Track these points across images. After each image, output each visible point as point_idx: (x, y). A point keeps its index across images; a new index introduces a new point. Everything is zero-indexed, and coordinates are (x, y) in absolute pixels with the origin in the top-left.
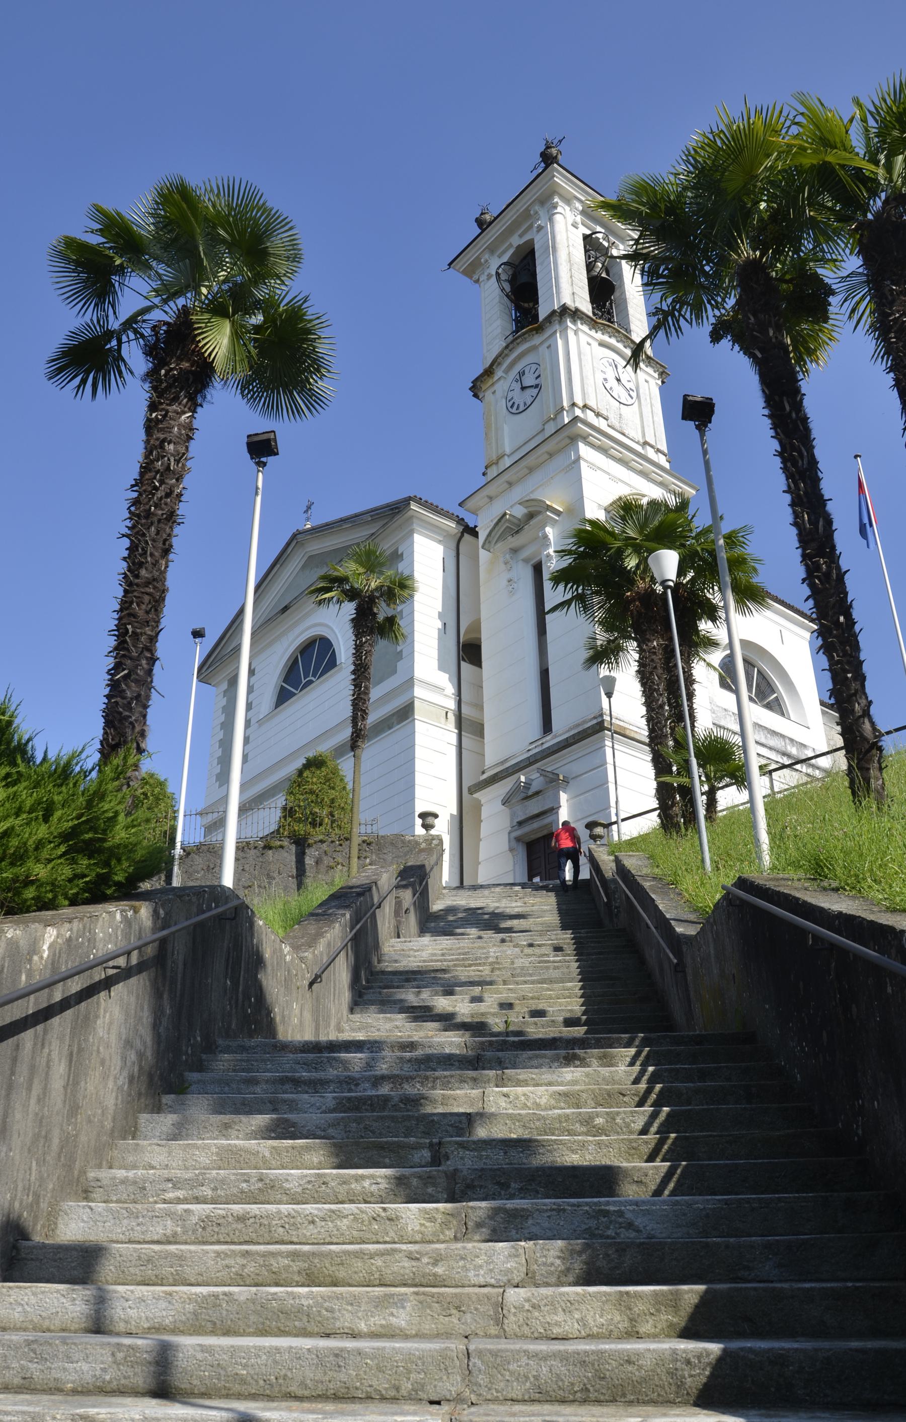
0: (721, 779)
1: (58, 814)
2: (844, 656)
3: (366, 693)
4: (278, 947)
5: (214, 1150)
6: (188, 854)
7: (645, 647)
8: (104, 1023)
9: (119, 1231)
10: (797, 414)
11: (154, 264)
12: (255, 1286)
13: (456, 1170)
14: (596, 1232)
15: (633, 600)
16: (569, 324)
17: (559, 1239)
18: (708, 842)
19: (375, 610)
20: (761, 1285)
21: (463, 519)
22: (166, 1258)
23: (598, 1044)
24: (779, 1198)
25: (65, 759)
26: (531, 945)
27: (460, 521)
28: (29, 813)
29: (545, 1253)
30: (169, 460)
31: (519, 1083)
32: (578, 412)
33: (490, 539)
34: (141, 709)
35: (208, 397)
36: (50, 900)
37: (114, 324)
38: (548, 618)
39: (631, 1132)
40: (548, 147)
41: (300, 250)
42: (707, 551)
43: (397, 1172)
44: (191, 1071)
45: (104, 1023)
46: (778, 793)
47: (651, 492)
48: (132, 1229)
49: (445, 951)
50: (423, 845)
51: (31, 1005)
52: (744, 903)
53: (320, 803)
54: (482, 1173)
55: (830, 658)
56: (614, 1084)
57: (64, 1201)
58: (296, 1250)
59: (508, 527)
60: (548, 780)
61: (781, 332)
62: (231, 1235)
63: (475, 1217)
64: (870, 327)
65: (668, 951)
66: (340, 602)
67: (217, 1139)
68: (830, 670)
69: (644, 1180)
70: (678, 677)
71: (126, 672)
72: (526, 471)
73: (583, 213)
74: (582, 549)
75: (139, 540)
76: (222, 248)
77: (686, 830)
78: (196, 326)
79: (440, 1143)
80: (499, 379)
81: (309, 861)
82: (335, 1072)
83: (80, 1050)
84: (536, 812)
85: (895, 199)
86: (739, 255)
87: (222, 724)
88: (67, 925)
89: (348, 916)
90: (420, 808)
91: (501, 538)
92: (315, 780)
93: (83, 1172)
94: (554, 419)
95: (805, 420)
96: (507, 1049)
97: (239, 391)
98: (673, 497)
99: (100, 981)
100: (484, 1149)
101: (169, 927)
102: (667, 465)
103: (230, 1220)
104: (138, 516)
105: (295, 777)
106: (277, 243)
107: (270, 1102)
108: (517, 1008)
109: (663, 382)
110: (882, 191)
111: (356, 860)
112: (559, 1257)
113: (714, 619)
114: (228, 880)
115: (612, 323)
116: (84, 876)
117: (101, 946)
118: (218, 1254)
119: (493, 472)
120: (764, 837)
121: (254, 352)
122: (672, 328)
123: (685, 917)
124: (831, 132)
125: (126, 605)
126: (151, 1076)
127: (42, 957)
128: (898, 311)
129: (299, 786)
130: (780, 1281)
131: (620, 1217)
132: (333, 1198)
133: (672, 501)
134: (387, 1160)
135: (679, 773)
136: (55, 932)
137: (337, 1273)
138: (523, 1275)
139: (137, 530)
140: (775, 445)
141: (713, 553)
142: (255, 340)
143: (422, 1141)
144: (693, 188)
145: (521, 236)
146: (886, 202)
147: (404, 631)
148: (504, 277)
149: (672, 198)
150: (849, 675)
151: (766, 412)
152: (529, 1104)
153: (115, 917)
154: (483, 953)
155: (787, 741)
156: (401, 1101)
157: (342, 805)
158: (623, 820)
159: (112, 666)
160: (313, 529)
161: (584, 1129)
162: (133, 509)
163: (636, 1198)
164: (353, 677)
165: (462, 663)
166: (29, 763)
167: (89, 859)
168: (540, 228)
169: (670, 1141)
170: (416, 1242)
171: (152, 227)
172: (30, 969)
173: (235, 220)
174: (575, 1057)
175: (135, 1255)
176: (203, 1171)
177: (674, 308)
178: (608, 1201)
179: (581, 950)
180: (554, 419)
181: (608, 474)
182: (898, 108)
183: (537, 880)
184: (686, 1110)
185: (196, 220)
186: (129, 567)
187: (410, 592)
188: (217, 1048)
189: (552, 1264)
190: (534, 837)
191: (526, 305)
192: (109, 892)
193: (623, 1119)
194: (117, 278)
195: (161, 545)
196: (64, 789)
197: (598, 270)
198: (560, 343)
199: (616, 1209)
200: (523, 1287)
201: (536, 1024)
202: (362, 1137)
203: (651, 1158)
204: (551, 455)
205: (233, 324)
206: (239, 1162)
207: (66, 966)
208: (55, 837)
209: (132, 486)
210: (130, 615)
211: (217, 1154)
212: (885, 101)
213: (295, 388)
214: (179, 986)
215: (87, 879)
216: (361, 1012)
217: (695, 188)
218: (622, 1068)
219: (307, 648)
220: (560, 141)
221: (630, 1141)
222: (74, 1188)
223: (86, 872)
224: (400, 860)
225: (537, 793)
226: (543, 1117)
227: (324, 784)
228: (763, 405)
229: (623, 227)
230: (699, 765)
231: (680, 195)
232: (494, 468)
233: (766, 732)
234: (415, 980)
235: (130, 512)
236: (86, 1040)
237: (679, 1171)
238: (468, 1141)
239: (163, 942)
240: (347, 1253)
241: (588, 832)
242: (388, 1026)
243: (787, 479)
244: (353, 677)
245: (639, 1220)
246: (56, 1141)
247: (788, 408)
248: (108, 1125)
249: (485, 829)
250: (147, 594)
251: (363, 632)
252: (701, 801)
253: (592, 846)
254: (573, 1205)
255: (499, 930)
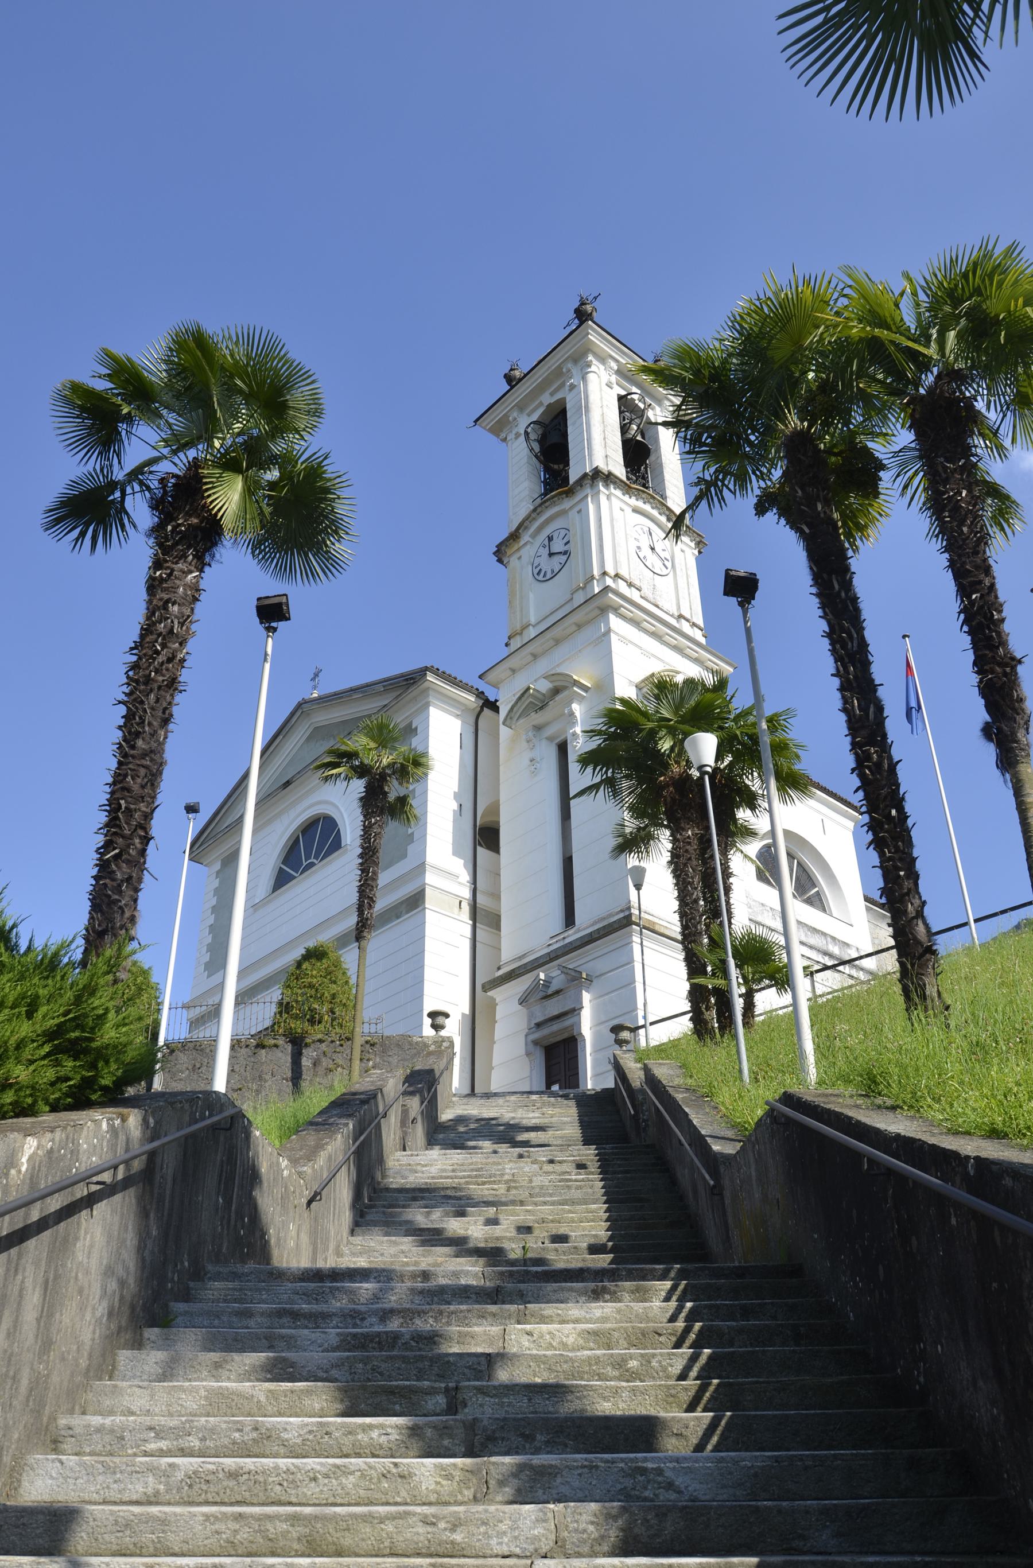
0: (760, 981)
1: (43, 1010)
2: (896, 852)
3: (374, 879)
4: (275, 1160)
5: (203, 1393)
6: (172, 1051)
7: (678, 836)
8: (84, 1245)
9: (93, 1489)
10: (846, 594)
11: (164, 412)
12: (248, 1556)
13: (475, 1420)
14: (633, 1493)
15: (667, 785)
16: (602, 488)
17: (592, 1501)
18: (747, 1050)
19: (386, 789)
20: (820, 1558)
21: (483, 693)
22: (147, 1522)
23: (630, 1276)
24: (834, 1455)
25: (53, 948)
26: (551, 1162)
27: (480, 694)
28: (12, 1008)
29: (577, 1517)
30: (172, 622)
31: (544, 1320)
32: (609, 582)
33: (512, 714)
34: (132, 893)
35: (217, 556)
36: (29, 1105)
37: (119, 475)
38: (573, 803)
39: (668, 1377)
40: (583, 304)
41: (320, 404)
42: (747, 734)
43: (409, 1421)
44: (176, 1301)
45: (84, 1245)
46: (820, 996)
47: (685, 670)
48: (108, 1487)
49: (455, 1167)
50: (432, 1048)
51: (6, 1225)
52: (789, 1121)
53: (320, 999)
54: (504, 1423)
55: (881, 855)
56: (647, 1322)
57: (29, 1453)
58: (296, 1512)
59: (531, 702)
60: (569, 977)
61: (829, 506)
62: (221, 1494)
63: (495, 1474)
64: (924, 504)
65: (704, 1171)
66: (347, 778)
67: (206, 1380)
68: (881, 867)
69: (685, 1433)
70: (714, 869)
71: (117, 851)
72: (552, 643)
73: (619, 372)
74: (612, 730)
75: (137, 708)
76: (239, 399)
77: (722, 1036)
78: (205, 480)
79: (457, 1388)
80: (525, 544)
81: (306, 1062)
82: (338, 1304)
83: (57, 1277)
84: (556, 1013)
85: (947, 375)
86: (786, 426)
87: (214, 907)
88: (49, 1135)
89: (351, 1126)
90: (429, 1007)
91: (524, 714)
92: (314, 972)
93: (53, 1419)
94: (583, 588)
95: (855, 599)
96: (529, 1281)
97: (250, 551)
98: (711, 676)
99: (82, 1198)
100: (506, 1395)
101: (159, 1138)
102: (703, 641)
103: (221, 1476)
104: (137, 681)
105: (293, 969)
106: (298, 397)
107: (266, 1338)
108: (536, 1233)
109: (700, 552)
110: (934, 366)
111: (358, 1062)
112: (592, 1523)
113: (753, 807)
114: (220, 1085)
115: (647, 488)
116: (67, 1079)
117: (84, 1159)
118: (207, 1517)
119: (516, 643)
120: (809, 1046)
121: (267, 510)
122: (715, 499)
123: (722, 1134)
124: (880, 305)
125: (120, 778)
126: (133, 1308)
127: (19, 1171)
128: (952, 490)
129: (297, 979)
130: (839, 1553)
131: (659, 1475)
132: (336, 1450)
133: (710, 680)
134: (397, 1407)
135: (714, 974)
136: (35, 1143)
137: (342, 1539)
138: (552, 1544)
139: (135, 696)
140: (824, 626)
141: (754, 739)
142: (270, 497)
143: (437, 1385)
144: (738, 354)
145: (552, 394)
146: (939, 377)
147: (417, 812)
148: (533, 436)
149: (716, 364)
150: (902, 873)
151: (814, 590)
152: (554, 1344)
153: (101, 1126)
154: (498, 1170)
155: (829, 939)
156: (413, 1339)
157: (344, 1001)
158: (652, 1024)
159: (102, 843)
160: (320, 699)
161: (616, 1373)
162: (131, 673)
163: (676, 1453)
164: (360, 861)
165: (478, 848)
166: (12, 951)
167: (74, 1061)
168: (572, 387)
169: (712, 1388)
170: (430, 1504)
171: (164, 374)
172: (7, 1184)
173: (254, 371)
174: (604, 1290)
175: (111, 1518)
176: (191, 1418)
177: (717, 478)
178: (646, 1458)
179: (606, 1168)
180: (583, 588)
181: (641, 648)
182: (949, 283)
183: (555, 1088)
184: (729, 1353)
185: (212, 370)
186: (124, 736)
187: (424, 770)
188: (205, 1274)
189: (585, 1531)
190: (553, 1040)
191: (556, 467)
192: (94, 1097)
193: (660, 1362)
194: (125, 426)
195: (160, 714)
196: (50, 981)
197: (633, 432)
198: (591, 507)
199: (655, 1466)
200: (552, 1557)
201: (557, 1250)
202: (369, 1380)
203: (691, 1408)
204: (579, 626)
205: (245, 480)
206: (231, 1408)
207: (46, 1182)
208: (38, 1036)
209: (132, 649)
210: (123, 789)
211: (206, 1398)
212: (936, 276)
213: (310, 550)
214: (167, 1204)
215: (72, 1083)
216: (363, 1234)
217: (740, 354)
218: (656, 1304)
219: (309, 828)
220: (595, 298)
221: (668, 1387)
222: (42, 1438)
223: (71, 1075)
224: (406, 1063)
225: (558, 992)
226: (571, 1359)
227: (325, 977)
228: (811, 583)
229: (665, 392)
230: (737, 966)
231: (725, 362)
232: (518, 638)
233: (806, 929)
234: (423, 1198)
235: (128, 677)
236: (63, 1266)
237: (723, 1423)
238: (488, 1386)
239: (152, 1155)
240: (354, 1516)
241: (613, 1036)
242: (393, 1250)
243: (836, 662)
244: (360, 861)
245: (680, 1480)
246: (24, 1383)
247: (837, 586)
248: (83, 1363)
249: (500, 1030)
250: (143, 766)
251: (373, 812)
252: (739, 1004)
253: (618, 1052)
254: (607, 1461)
255: (515, 1144)
